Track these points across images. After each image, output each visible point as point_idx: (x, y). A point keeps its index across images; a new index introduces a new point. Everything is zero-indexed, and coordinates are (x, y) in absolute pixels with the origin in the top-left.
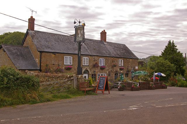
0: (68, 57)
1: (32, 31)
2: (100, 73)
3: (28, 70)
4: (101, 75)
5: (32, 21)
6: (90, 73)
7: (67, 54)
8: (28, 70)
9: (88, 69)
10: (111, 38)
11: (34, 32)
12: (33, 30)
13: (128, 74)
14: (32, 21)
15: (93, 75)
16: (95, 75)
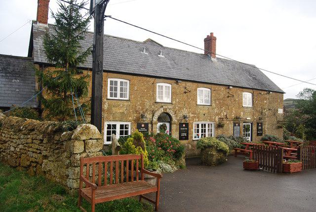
0: (119, 81)
1: (41, 24)
2: (199, 121)
3: (233, 86)
4: (202, 125)
5: (210, 42)
6: (174, 120)
7: (115, 75)
8: (233, 86)
9: (168, 111)
10: (105, 21)
11: (46, 26)
12: (46, 23)
13: (261, 123)
14: (210, 42)
15: (181, 125)
16: (187, 125)
